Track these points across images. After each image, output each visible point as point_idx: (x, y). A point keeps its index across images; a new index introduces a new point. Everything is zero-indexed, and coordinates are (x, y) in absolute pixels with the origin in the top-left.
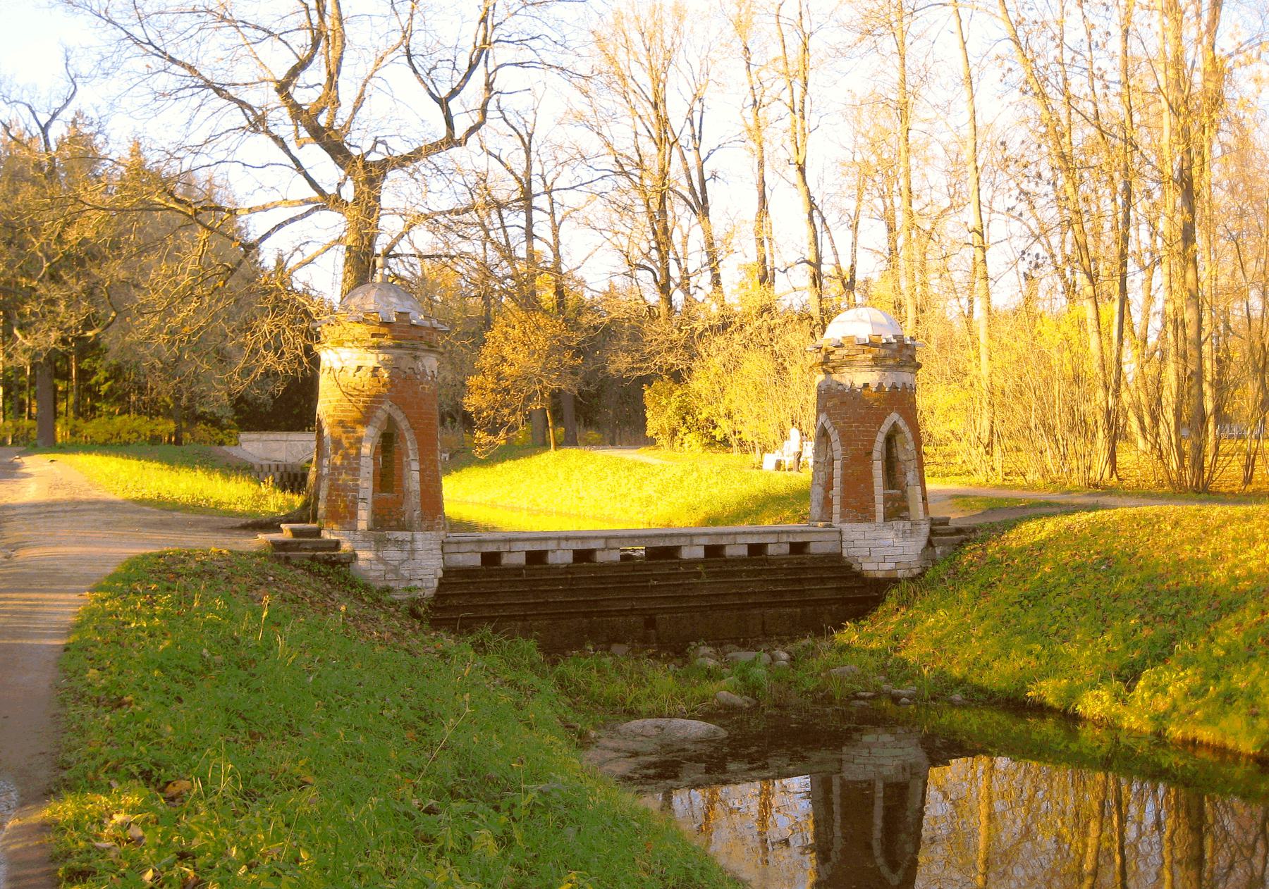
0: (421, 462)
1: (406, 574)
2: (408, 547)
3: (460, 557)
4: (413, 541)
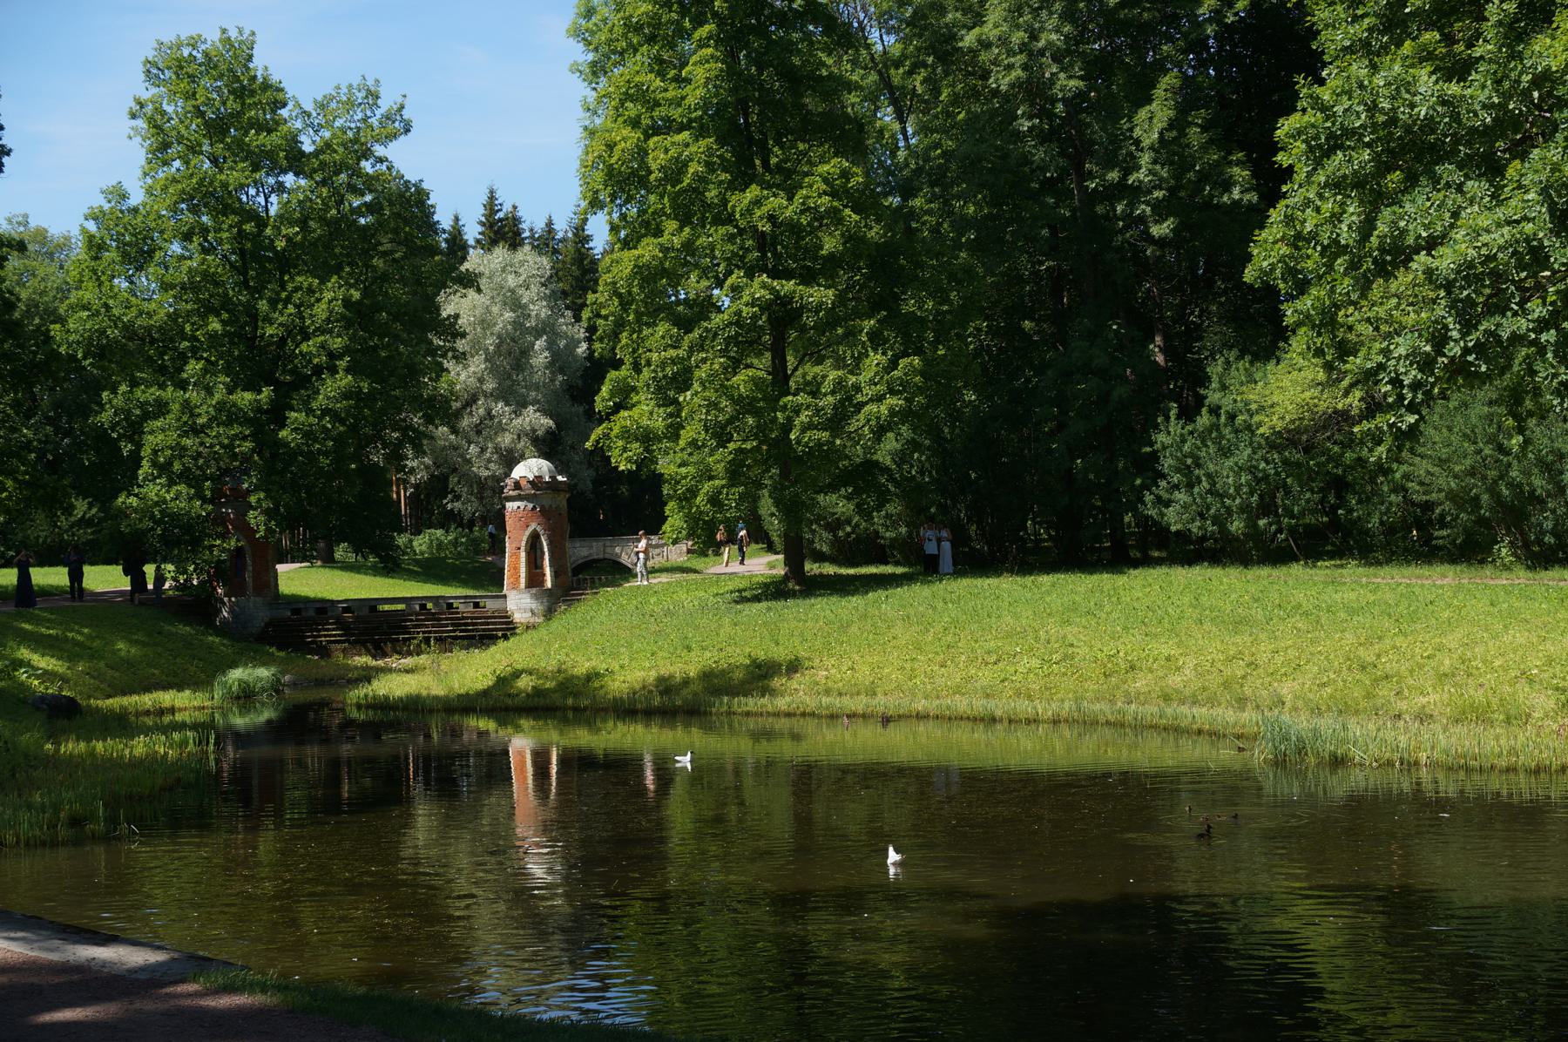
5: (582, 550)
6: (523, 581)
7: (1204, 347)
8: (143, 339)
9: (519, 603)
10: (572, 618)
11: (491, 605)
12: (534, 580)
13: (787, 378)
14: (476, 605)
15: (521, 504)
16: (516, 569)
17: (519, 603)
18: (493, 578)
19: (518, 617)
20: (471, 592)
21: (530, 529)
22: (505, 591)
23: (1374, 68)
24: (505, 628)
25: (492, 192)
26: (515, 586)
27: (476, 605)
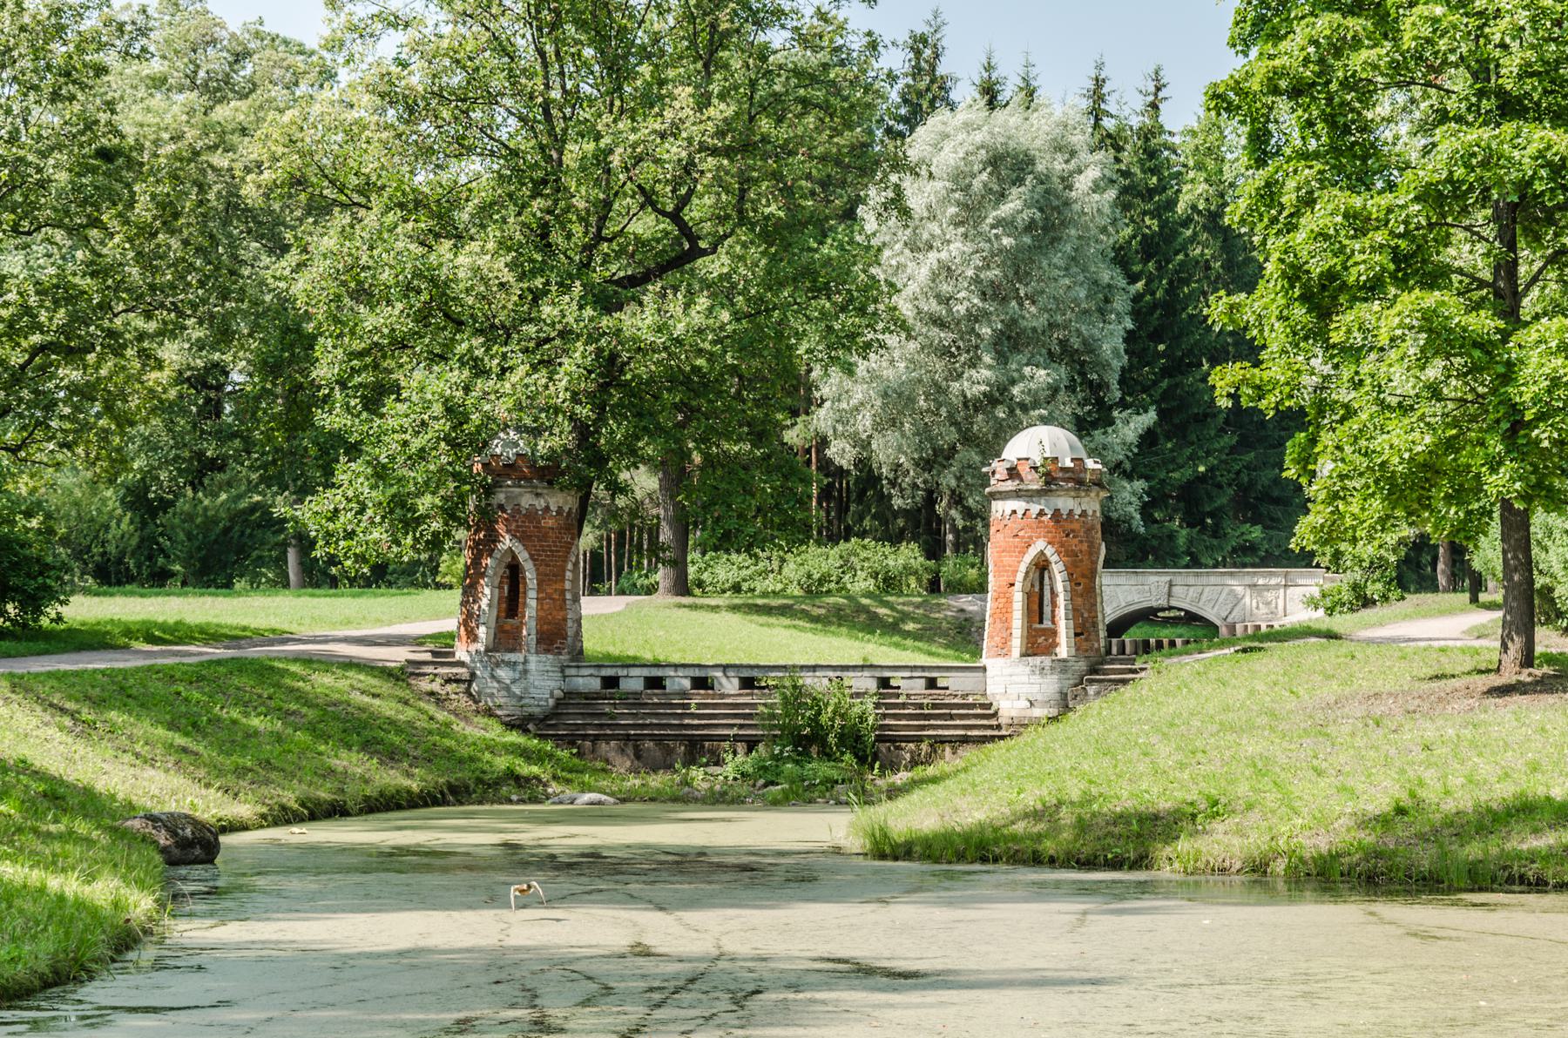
0: (540, 589)
1: (518, 692)
2: (520, 667)
3: (580, 680)
4: (526, 662)
5: (1123, 591)
6: (1017, 643)
7: (81, 146)
8: (204, 215)
9: (1010, 681)
10: (1102, 713)
11: (956, 683)
12: (1038, 642)
13: (1517, 297)
14: (932, 683)
15: (1019, 505)
16: (1007, 624)
17: (1010, 681)
18: (966, 634)
19: (1009, 708)
20: (922, 660)
21: (1032, 553)
22: (985, 661)
23: (465, 436)
24: (981, 728)
25: (1099, 83)
26: (1003, 650)
27: (932, 683)
